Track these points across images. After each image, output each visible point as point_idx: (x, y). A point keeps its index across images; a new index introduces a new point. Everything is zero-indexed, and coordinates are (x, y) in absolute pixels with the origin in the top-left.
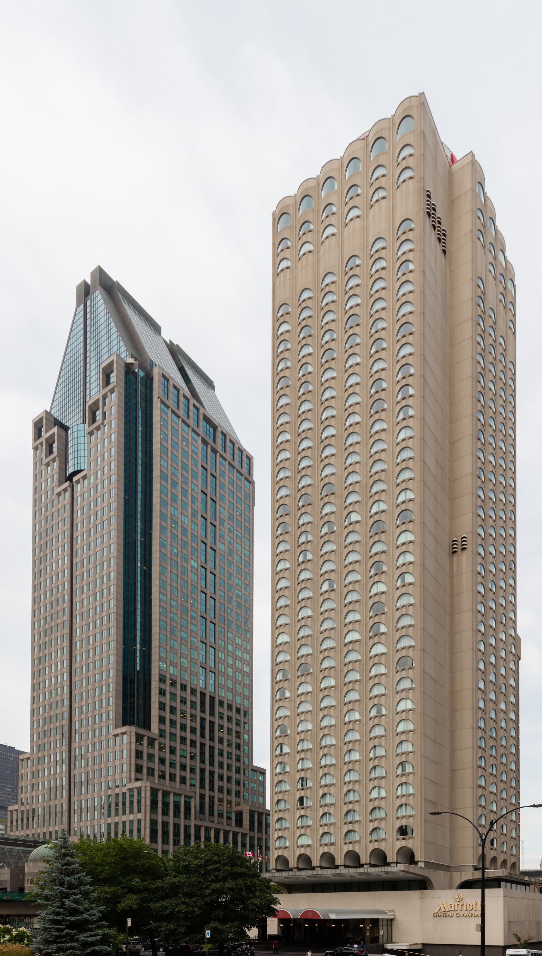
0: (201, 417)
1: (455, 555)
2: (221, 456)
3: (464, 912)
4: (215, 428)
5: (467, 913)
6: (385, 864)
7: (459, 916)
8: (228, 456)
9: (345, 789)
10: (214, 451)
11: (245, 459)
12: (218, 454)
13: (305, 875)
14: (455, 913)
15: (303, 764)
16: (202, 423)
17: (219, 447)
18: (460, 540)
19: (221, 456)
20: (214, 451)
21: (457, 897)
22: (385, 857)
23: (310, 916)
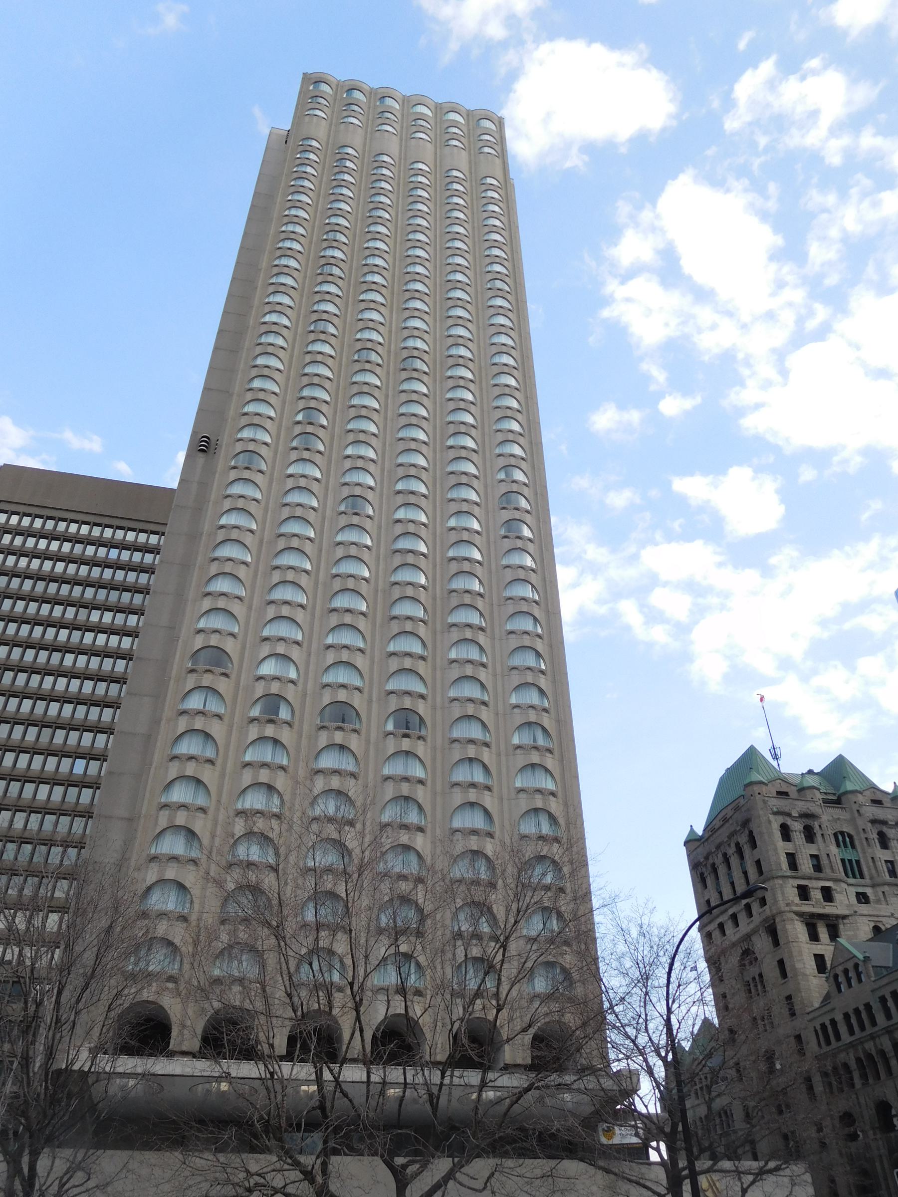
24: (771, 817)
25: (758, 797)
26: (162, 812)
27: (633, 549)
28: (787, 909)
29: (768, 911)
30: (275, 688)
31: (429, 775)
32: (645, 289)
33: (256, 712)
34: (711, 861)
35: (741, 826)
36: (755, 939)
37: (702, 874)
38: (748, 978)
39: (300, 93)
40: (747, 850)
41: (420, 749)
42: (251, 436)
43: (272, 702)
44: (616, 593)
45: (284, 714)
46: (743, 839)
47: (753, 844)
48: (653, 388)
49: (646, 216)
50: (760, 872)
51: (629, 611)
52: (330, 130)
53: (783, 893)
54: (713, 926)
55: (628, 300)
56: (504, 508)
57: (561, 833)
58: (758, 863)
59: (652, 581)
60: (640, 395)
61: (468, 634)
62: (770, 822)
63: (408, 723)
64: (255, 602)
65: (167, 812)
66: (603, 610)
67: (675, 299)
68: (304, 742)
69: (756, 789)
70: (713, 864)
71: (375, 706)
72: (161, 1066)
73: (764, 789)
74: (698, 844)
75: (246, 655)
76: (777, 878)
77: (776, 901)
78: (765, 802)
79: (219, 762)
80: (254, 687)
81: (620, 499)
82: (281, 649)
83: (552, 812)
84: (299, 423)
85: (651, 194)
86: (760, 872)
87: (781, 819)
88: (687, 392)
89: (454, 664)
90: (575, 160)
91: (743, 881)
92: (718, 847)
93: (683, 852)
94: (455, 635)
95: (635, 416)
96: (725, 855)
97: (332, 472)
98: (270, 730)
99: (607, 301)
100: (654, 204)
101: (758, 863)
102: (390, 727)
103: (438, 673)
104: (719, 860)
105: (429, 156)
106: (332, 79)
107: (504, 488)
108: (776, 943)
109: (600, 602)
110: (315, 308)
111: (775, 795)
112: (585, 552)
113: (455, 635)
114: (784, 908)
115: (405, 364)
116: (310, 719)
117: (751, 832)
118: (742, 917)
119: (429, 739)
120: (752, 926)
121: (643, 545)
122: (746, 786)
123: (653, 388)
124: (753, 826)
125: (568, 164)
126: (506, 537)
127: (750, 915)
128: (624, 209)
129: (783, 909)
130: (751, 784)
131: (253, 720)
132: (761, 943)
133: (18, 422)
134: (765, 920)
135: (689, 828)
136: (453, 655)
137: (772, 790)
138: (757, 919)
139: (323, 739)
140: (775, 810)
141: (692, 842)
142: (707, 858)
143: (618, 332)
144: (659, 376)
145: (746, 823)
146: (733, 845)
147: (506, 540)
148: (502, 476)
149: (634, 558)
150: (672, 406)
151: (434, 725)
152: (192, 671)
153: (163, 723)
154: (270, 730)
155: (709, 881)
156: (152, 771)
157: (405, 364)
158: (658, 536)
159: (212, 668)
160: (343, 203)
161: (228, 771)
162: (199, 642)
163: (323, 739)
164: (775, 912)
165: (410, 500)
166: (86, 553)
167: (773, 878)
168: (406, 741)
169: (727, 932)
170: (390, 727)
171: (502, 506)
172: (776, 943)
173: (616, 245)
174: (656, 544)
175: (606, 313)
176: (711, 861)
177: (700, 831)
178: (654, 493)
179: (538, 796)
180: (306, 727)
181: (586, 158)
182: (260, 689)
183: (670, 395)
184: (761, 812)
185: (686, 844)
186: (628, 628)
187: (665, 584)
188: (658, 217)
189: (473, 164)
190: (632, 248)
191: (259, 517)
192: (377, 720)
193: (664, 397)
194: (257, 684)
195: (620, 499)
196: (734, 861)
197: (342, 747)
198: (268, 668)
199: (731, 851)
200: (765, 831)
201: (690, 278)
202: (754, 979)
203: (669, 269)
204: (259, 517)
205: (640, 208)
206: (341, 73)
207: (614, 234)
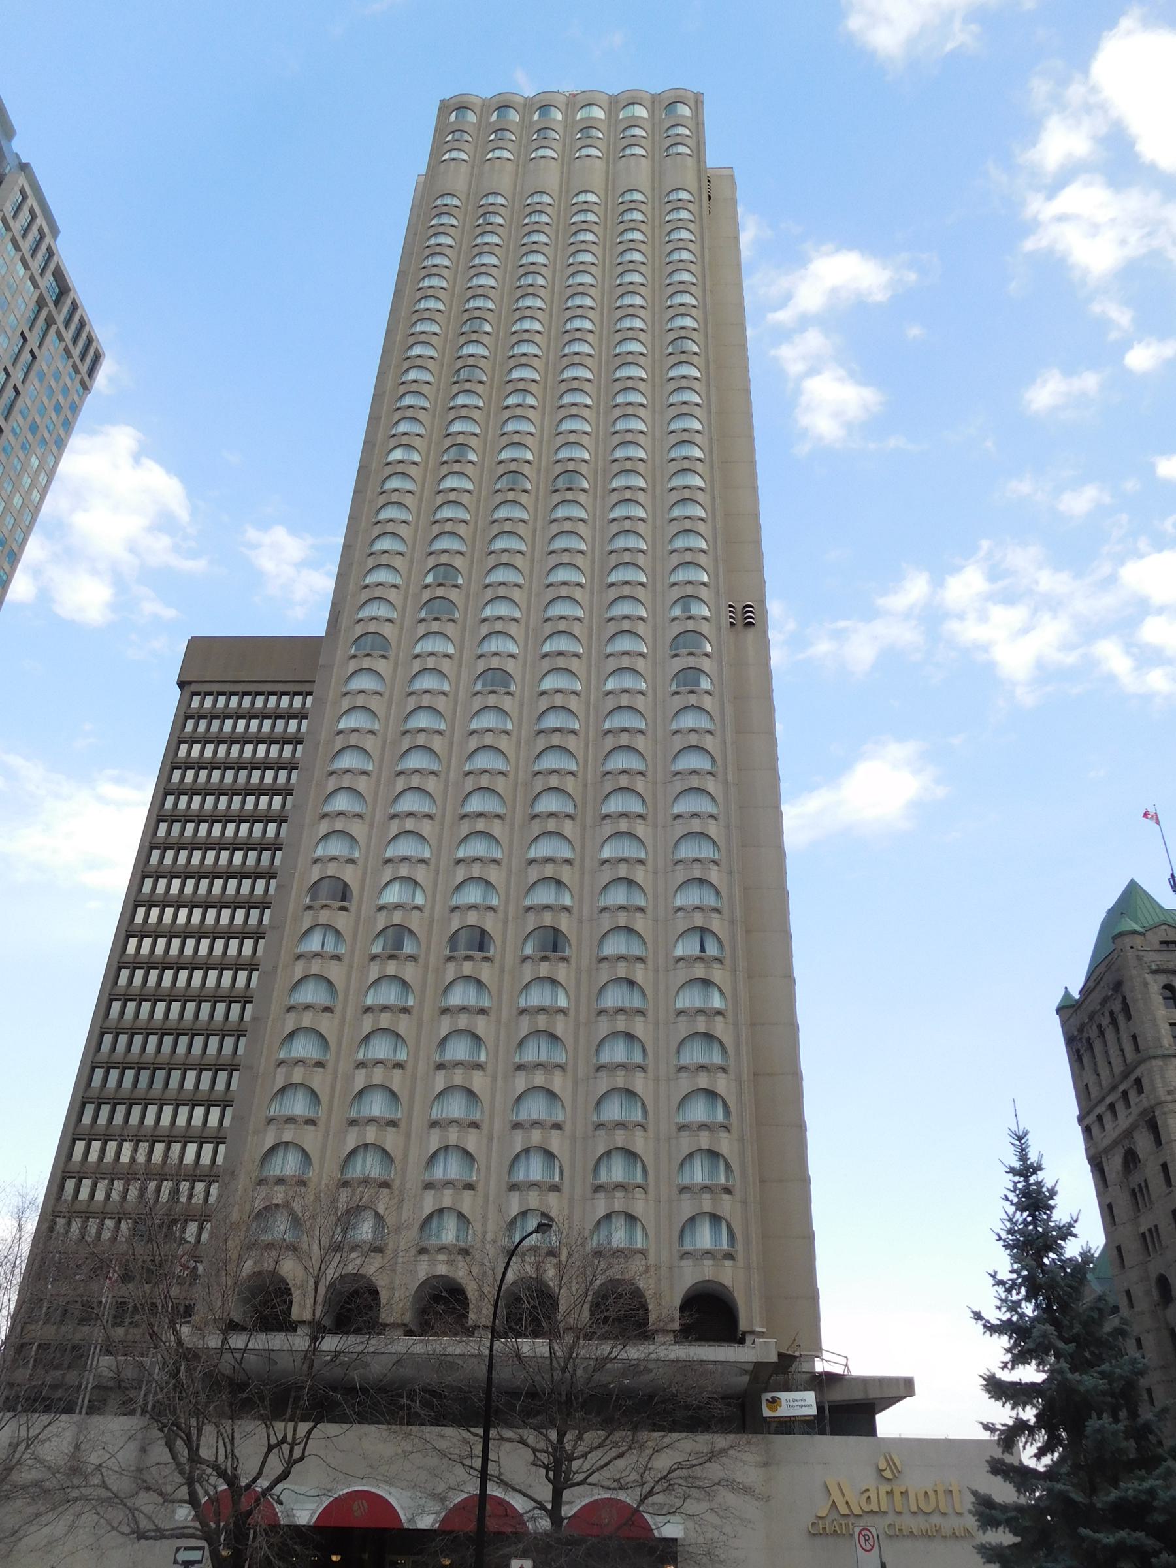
24: (1149, 978)
25: (1130, 952)
26: (279, 1070)
27: (1106, 569)
28: (1169, 1098)
29: (1145, 1101)
30: (397, 918)
31: (573, 1004)
32: (1086, 198)
33: (377, 948)
34: (1085, 1035)
35: (1113, 989)
36: (1136, 1135)
37: (1078, 1051)
38: (1134, 1185)
39: (436, 131)
40: (1121, 1018)
41: (562, 973)
44: (1090, 631)
45: (409, 948)
46: (1117, 1006)
47: (1128, 1017)
48: (1113, 336)
49: (1075, 92)
50: (1137, 1050)
51: (1113, 656)
52: (472, 175)
53: (1163, 1077)
54: (1091, 1118)
55: (1061, 218)
56: (675, 656)
57: (392, 1175)
58: (1134, 1037)
59: (1142, 608)
60: (1100, 350)
61: (623, 825)
62: (1146, 984)
63: (553, 942)
64: (377, 818)
65: (284, 1070)
66: (1071, 659)
67: (1134, 201)
68: (430, 980)
69: (1128, 941)
70: (1089, 1038)
71: (511, 926)
73: (1138, 941)
74: (1071, 1011)
75: (368, 881)
76: (1154, 1058)
77: (1154, 1089)
78: (1139, 958)
80: (375, 918)
81: (1080, 502)
82: (404, 871)
83: (388, 1149)
84: (427, 586)
85: (1080, 56)
86: (1137, 1050)
87: (1163, 979)
88: (1163, 334)
89: (606, 866)
90: (961, 37)
91: (1120, 1060)
92: (1091, 1017)
93: (1056, 1020)
94: (608, 828)
95: (1090, 381)
96: (1099, 1026)
97: (466, 643)
99: (1031, 227)
100: (1085, 69)
101: (1134, 1038)
102: (529, 950)
103: (587, 877)
104: (1093, 1033)
105: (598, 181)
106: (474, 99)
107: (676, 628)
108: (1158, 1141)
109: (1066, 646)
110: (618, 327)
111: (1157, 946)
112: (1037, 583)
113: (608, 828)
114: (1164, 1096)
115: (564, 481)
116: (439, 947)
117: (1124, 998)
118: (1120, 1107)
119: (573, 961)
120: (1131, 1120)
121: (1121, 562)
122: (1115, 938)
123: (1113, 336)
124: (1126, 989)
125: (949, 46)
126: (677, 693)
127: (1128, 1106)
128: (1040, 87)
129: (1163, 1099)
130: (1121, 935)
131: (374, 958)
132: (1143, 1143)
133: (294, 531)
134: (1144, 1113)
135: (1063, 992)
136: (606, 853)
137: (1154, 939)
138: (1135, 1111)
139: (450, 972)
140: (1154, 967)
141: (1067, 1009)
142: (1081, 1030)
143: (1053, 267)
144: (1122, 317)
145: (1118, 986)
146: (1107, 1014)
147: (676, 697)
148: (677, 611)
149: (1111, 581)
150: (1141, 358)
152: (310, 907)
153: (279, 970)
154: (391, 968)
155: (1086, 1059)
156: (270, 1023)
157: (564, 481)
158: (1143, 544)
159: (328, 902)
162: (315, 874)
163: (450, 972)
164: (1153, 1102)
165: (558, 663)
166: (289, 730)
167: (1150, 1058)
169: (1107, 1126)
170: (529, 950)
171: (673, 653)
172: (1158, 1141)
173: (1034, 145)
174: (1141, 556)
175: (1030, 245)
176: (1085, 1035)
178: (1131, 485)
179: (701, 1018)
180: (432, 959)
181: (974, 28)
182: (381, 921)
183: (1140, 342)
184: (1134, 972)
185: (1058, 1011)
186: (1111, 678)
187: (1161, 610)
188: (1094, 90)
189: (657, 175)
190: (1061, 142)
191: (586, 604)
193: (1132, 347)
194: (379, 914)
195: (1080, 502)
196: (1110, 1034)
198: (393, 895)
199: (1105, 1021)
200: (1139, 996)
201: (1152, 167)
202: (1140, 1185)
203: (1118, 160)
204: (586, 604)
205: (1064, 81)
206: (484, 89)
207: (1030, 129)
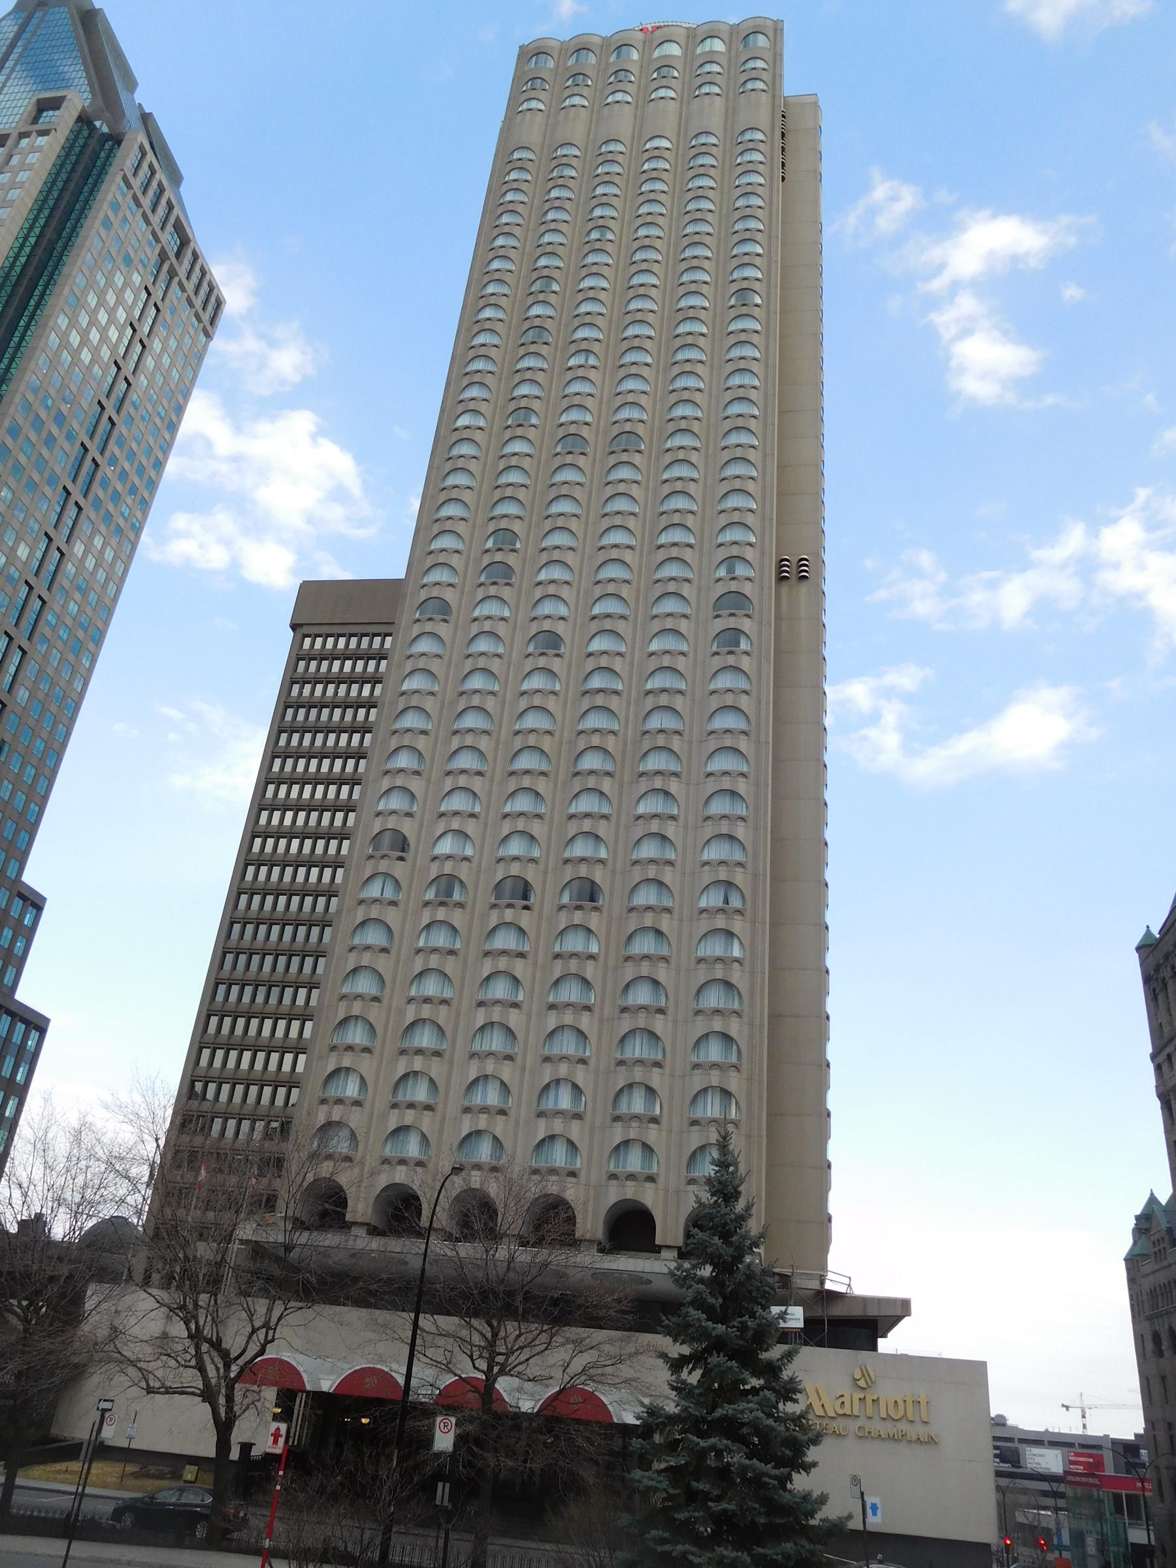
0: (172, 220)
1: (784, 583)
2: (181, 284)
3: (877, 1427)
4: (184, 241)
5: (885, 1429)
6: (493, 1235)
7: (865, 1436)
8: (190, 286)
9: (410, 1015)
10: (172, 273)
11: (213, 300)
12: (176, 280)
13: (404, 1250)
14: (853, 1425)
15: (427, 938)
16: (169, 227)
17: (182, 271)
18: (794, 560)
19: (181, 284)
20: (172, 273)
21: (858, 1375)
22: (342, 1202)
23: (369, 1388)
33: (430, 895)
37: (1154, 990)
42: (746, 204)
43: (447, 884)
70: (1164, 979)
71: (550, 876)
72: (558, 1258)
79: (394, 951)
98: (441, 914)
102: (566, 899)
116: (483, 895)
147: (716, 657)
148: (722, 572)
151: (612, 894)
154: (441, 914)
155: (1160, 998)
160: (621, 94)
161: (402, 958)
168: (578, 913)
170: (566, 899)
176: (1161, 975)
177: (1155, 932)
185: (1138, 949)
192: (545, 895)
194: (432, 864)
197: (732, 838)
198: (446, 847)
